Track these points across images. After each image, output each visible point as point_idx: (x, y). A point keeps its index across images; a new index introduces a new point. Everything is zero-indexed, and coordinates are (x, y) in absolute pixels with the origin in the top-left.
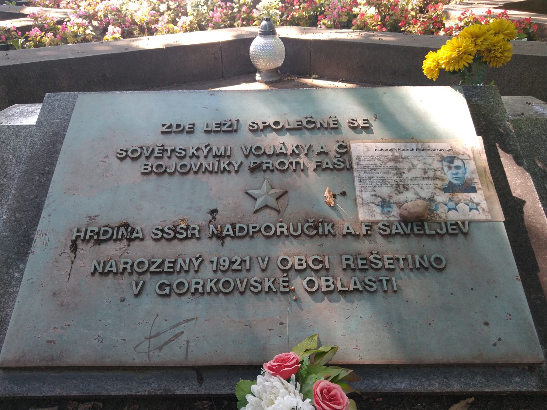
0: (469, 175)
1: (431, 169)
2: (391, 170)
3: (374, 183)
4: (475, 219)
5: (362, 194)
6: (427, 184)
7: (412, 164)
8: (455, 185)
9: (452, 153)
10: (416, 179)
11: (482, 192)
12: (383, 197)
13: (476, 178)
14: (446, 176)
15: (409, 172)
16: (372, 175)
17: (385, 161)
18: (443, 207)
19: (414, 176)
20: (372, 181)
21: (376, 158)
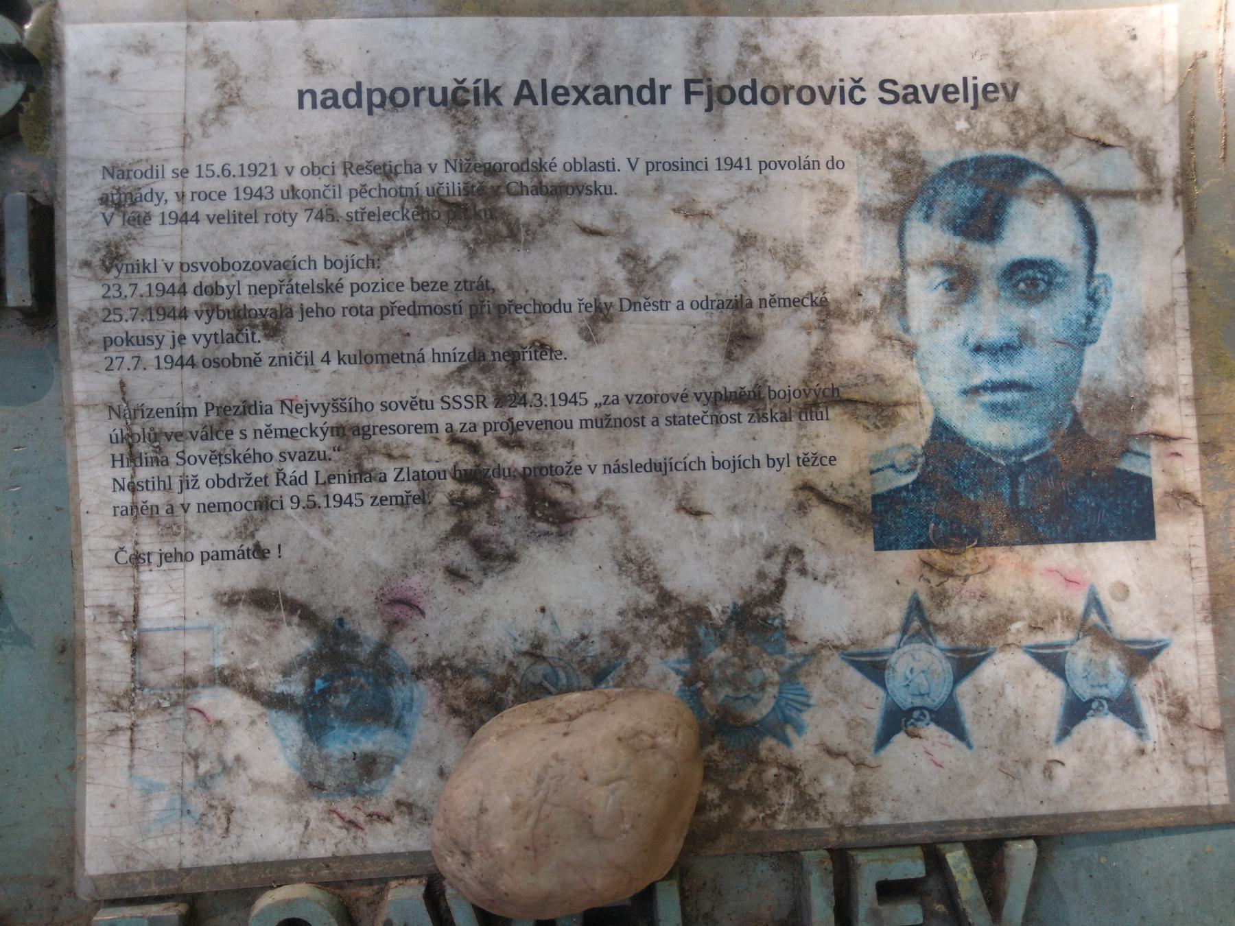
0: (1115, 353)
1: (796, 303)
2: (425, 324)
3: (258, 470)
4: (1098, 806)
5: (136, 592)
6: (737, 464)
7: (631, 257)
8: (982, 459)
9: (999, 128)
10: (652, 409)
11: (1200, 531)
12: (330, 616)
13: (1168, 391)
14: (914, 376)
15: (589, 337)
16: (244, 382)
17: (379, 230)
18: (841, 693)
19: (635, 381)
20: (240, 446)
21: (293, 192)
